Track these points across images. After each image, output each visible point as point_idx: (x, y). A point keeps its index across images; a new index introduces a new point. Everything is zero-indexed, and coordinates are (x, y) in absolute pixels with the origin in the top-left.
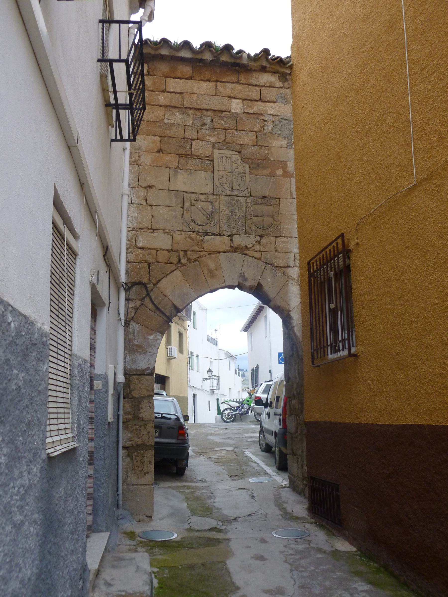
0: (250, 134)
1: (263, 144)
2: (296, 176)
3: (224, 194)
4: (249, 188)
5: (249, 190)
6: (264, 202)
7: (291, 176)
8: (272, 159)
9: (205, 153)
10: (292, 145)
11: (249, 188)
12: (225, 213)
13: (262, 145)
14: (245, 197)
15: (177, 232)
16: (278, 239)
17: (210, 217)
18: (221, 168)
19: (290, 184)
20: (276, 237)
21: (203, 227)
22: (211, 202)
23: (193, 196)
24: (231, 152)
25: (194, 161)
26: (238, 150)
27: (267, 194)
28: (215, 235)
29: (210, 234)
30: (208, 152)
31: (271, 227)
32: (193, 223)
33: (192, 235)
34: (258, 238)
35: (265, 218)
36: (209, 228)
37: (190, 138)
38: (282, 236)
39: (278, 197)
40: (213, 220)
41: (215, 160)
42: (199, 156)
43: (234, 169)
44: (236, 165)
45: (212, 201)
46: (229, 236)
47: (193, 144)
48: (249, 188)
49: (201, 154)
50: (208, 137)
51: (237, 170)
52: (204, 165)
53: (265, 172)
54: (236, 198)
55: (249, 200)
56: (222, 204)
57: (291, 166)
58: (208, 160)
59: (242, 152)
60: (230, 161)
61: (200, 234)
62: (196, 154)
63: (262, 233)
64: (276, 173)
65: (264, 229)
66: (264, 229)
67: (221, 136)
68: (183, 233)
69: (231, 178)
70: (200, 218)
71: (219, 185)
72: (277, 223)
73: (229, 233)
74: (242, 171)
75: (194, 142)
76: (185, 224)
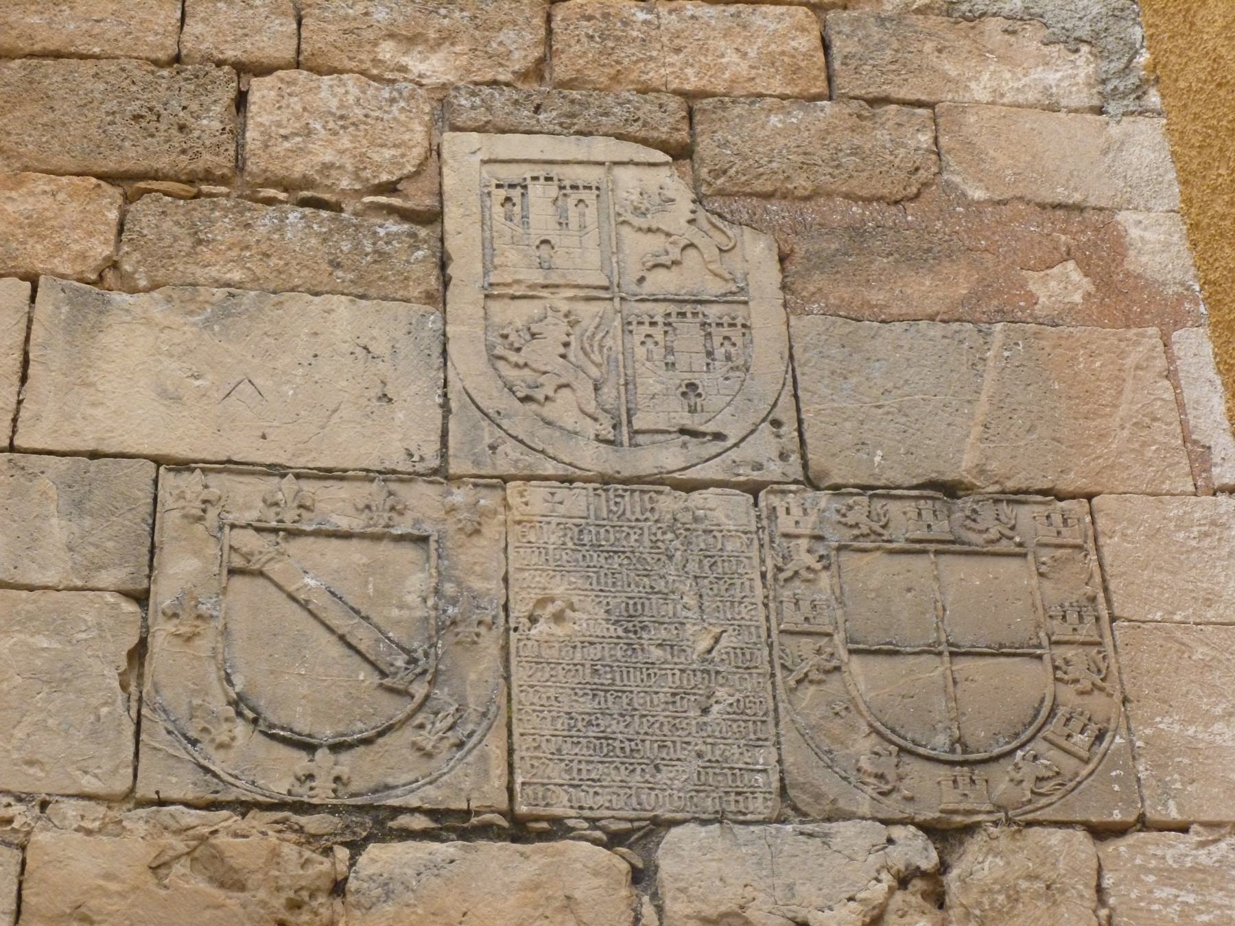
0: (758, 21)
1: (889, 90)
2: (1215, 304)
3: (550, 468)
4: (785, 413)
5: (789, 429)
6: (941, 528)
7: (1171, 318)
8: (978, 194)
9: (362, 160)
10: (1139, 91)
11: (789, 417)
12: (559, 631)
13: (874, 91)
14: (754, 489)
15: (70, 810)
16: (1121, 846)
17: (411, 673)
18: (517, 266)
19: (1170, 375)
20: (1101, 832)
21: (346, 763)
22: (424, 540)
23: (247, 498)
24: (602, 148)
25: (265, 219)
26: (663, 133)
27: (962, 467)
28: (467, 834)
29: (419, 822)
30: (388, 153)
31: (1039, 746)
32: (241, 729)
33: (222, 840)
34: (915, 850)
35: (963, 664)
36: (394, 771)
37: (231, 53)
38: (1151, 815)
39: (1070, 482)
40: (441, 694)
41: (451, 221)
42: (308, 183)
43: (634, 272)
44: (658, 242)
45: (428, 528)
46: (614, 840)
47: (254, 97)
48: (789, 417)
49: (327, 167)
50: (387, 51)
51: (662, 282)
52: (357, 246)
53: (923, 289)
54: (669, 502)
55: (798, 513)
56: (529, 555)
57: (1156, 242)
58: (391, 210)
59: (705, 146)
60: (591, 213)
61: (311, 823)
62: (277, 169)
63: (951, 799)
64: (1032, 300)
65: (966, 760)
66: (966, 760)
67: (508, 36)
68: (137, 821)
69: (614, 342)
70: (315, 684)
71: (495, 399)
72: (1098, 704)
73: (614, 803)
74: (714, 287)
75: (261, 90)
76: (156, 734)
